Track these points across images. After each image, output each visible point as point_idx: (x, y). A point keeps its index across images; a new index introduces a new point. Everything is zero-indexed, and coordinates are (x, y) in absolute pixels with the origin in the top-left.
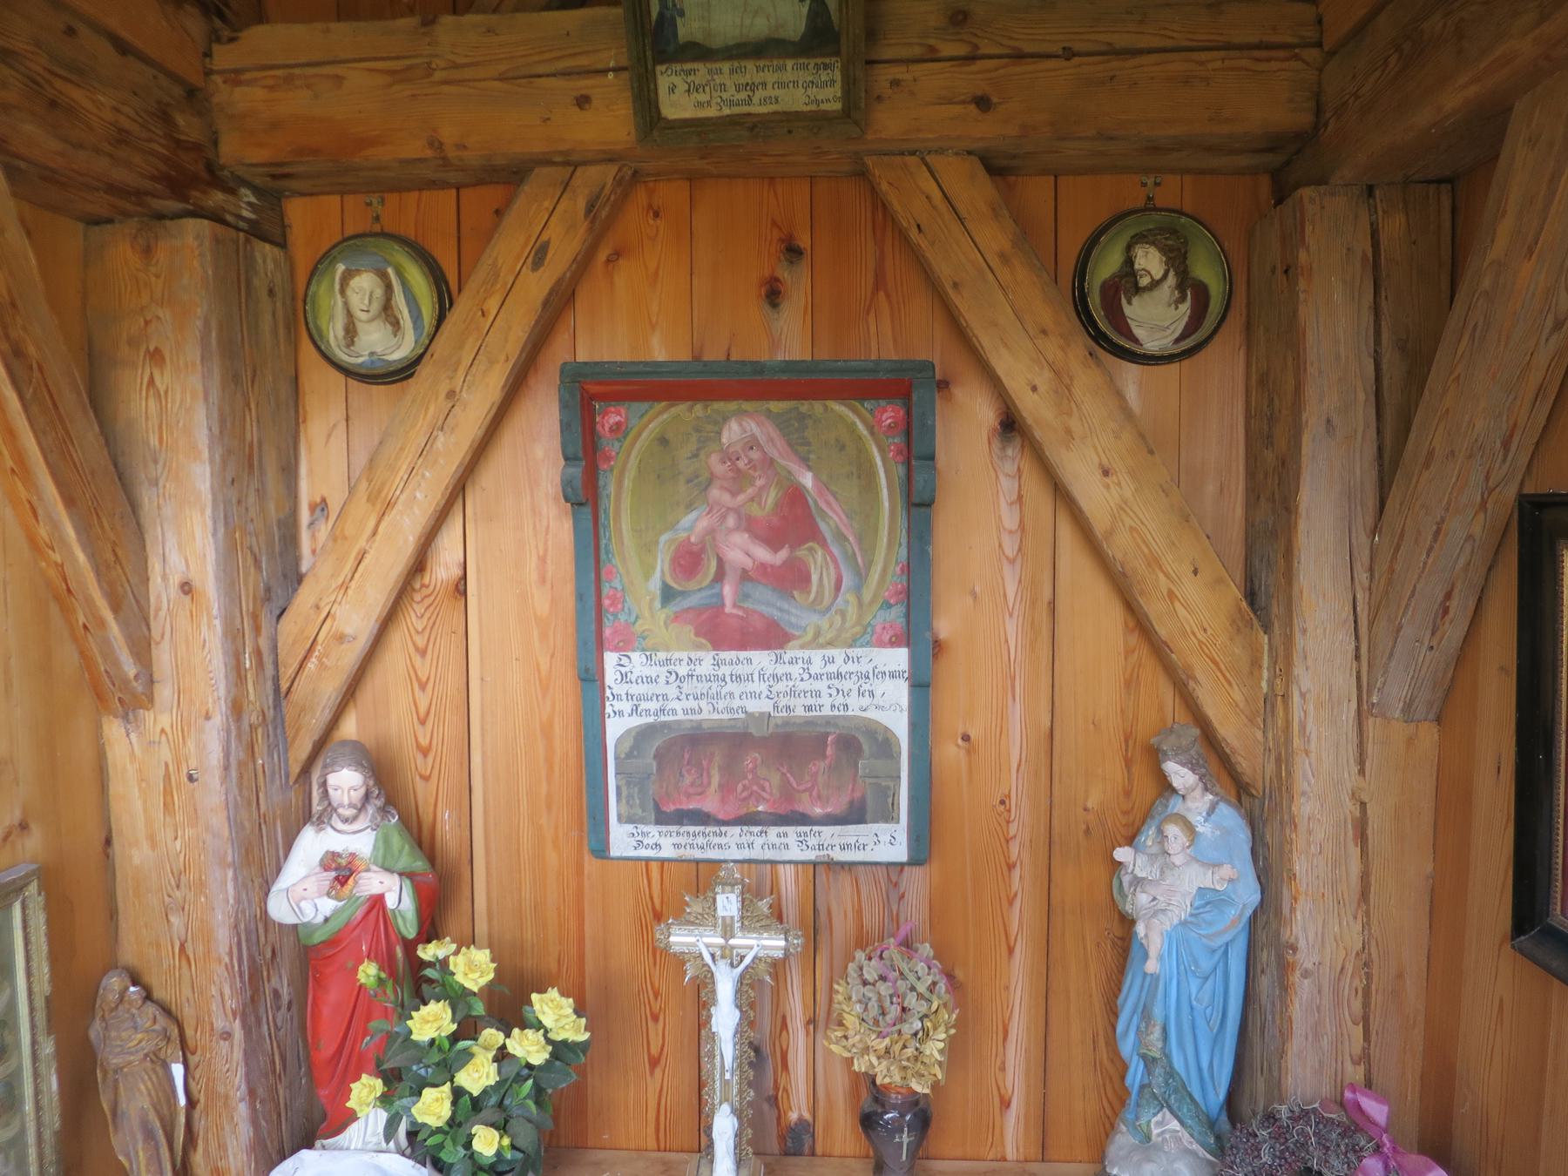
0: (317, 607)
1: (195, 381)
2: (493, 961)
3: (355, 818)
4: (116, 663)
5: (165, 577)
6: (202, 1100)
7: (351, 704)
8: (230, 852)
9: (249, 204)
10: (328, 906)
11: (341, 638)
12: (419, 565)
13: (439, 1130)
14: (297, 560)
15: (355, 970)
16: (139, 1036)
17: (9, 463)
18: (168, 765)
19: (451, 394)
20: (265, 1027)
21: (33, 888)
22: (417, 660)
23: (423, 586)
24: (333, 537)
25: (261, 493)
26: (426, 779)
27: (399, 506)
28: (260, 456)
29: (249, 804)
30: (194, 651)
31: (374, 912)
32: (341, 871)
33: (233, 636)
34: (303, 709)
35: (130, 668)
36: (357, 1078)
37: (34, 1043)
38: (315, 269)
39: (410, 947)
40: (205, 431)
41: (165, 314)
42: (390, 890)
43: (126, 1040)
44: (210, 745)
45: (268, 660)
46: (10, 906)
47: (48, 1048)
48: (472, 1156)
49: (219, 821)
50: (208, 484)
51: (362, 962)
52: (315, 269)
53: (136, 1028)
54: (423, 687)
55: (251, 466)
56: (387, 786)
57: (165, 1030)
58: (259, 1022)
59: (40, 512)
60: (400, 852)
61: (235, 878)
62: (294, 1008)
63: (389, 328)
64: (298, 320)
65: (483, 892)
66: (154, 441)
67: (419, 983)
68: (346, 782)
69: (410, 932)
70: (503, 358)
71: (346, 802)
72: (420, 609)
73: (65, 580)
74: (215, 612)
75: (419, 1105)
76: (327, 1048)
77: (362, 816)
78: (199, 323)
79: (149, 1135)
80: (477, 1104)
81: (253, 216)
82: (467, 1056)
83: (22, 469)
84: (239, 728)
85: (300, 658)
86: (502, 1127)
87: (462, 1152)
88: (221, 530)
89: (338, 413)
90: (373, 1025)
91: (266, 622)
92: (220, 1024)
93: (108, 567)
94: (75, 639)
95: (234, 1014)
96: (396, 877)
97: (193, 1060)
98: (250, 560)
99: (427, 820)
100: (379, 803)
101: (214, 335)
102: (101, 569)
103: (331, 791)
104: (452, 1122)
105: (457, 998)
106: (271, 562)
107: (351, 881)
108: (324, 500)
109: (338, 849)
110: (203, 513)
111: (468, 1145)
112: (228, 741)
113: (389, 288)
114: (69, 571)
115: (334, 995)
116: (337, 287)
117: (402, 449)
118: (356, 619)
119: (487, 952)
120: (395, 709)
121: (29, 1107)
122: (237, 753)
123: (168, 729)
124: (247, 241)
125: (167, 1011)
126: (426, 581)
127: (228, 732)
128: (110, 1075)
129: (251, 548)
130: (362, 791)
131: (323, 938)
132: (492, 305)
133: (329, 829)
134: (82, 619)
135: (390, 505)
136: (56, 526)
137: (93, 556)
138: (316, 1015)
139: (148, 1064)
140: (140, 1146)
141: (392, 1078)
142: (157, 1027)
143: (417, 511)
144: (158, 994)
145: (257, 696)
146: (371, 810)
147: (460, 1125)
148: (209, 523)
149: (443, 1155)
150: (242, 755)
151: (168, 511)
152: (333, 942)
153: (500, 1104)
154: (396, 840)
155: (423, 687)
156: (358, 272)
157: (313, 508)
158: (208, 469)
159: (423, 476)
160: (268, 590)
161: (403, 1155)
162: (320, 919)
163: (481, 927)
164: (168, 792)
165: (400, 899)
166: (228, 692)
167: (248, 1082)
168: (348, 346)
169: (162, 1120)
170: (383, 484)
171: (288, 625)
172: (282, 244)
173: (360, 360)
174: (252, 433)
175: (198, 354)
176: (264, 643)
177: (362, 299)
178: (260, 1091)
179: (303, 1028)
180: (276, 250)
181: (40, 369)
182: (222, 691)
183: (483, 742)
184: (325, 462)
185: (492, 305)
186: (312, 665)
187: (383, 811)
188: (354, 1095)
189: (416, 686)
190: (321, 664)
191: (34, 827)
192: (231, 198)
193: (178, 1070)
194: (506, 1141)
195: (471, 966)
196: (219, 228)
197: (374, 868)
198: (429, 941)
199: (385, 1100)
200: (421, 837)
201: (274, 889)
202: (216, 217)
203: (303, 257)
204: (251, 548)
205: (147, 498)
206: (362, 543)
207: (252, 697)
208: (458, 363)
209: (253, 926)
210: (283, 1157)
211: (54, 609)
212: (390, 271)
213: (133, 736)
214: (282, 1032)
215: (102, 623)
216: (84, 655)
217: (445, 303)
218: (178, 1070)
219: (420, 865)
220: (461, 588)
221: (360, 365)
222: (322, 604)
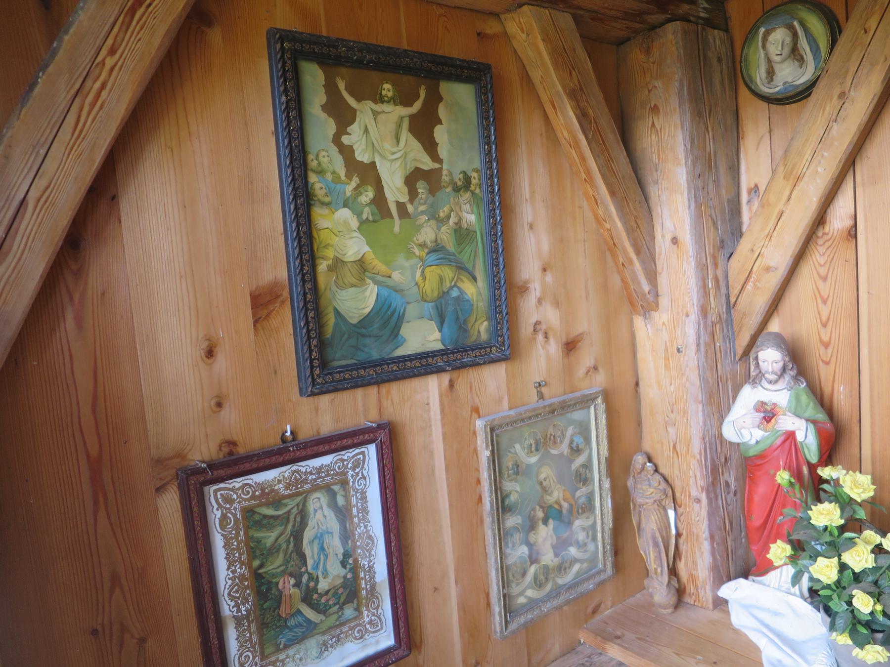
0: (752, 250)
1: (676, 119)
2: (873, 484)
3: (776, 382)
4: (639, 284)
5: (663, 236)
6: (684, 533)
7: (775, 313)
8: (700, 395)
9: (704, 8)
10: (759, 434)
11: (768, 269)
12: (820, 220)
13: (828, 587)
14: (740, 225)
15: (775, 475)
16: (652, 490)
17: (584, 176)
18: (667, 346)
19: (842, 95)
20: (720, 502)
21: (599, 400)
22: (821, 284)
23: (824, 234)
24: (762, 206)
25: (716, 182)
26: (827, 363)
27: (806, 179)
28: (717, 166)
29: (712, 369)
30: (679, 272)
31: (789, 440)
32: (768, 414)
33: (702, 267)
34: (744, 314)
35: (646, 287)
36: (775, 542)
37: (600, 480)
38: (747, 38)
39: (812, 468)
40: (682, 147)
41: (658, 84)
42: (799, 429)
43: (646, 492)
44: (689, 332)
45: (723, 283)
46: (589, 407)
47: (607, 484)
48: (852, 611)
49: (694, 377)
50: (685, 178)
51: (778, 470)
52: (747, 38)
53: (650, 485)
54: (825, 302)
55: (710, 166)
56: (797, 361)
57: (665, 490)
58: (717, 498)
59: (599, 201)
60: (807, 406)
61: (703, 411)
62: (738, 495)
63: (796, 63)
64: (737, 74)
65: (868, 439)
66: (655, 158)
67: (818, 489)
68: (770, 357)
69: (814, 459)
70: (882, 59)
71: (770, 370)
72: (822, 250)
73: (612, 238)
74: (691, 253)
75: (815, 566)
76: (757, 520)
77: (781, 381)
78: (677, 84)
79: (656, 544)
80: (857, 578)
81: (707, 16)
82: (851, 543)
83: (590, 179)
84: (705, 323)
85: (742, 282)
86: (878, 596)
87: (845, 607)
88: (693, 205)
89: (764, 128)
90: (785, 511)
91: (721, 261)
92: (694, 493)
93: (633, 230)
94: (619, 272)
95: (702, 489)
96: (804, 422)
97: (680, 510)
98: (710, 223)
99: (827, 390)
100: (793, 373)
101: (685, 88)
102: (630, 231)
103: (760, 363)
104: (838, 583)
105: (846, 504)
106: (724, 225)
107: (773, 421)
108: (756, 186)
109: (766, 400)
110: (682, 195)
111: (849, 603)
112: (699, 330)
113: (795, 35)
114: (614, 234)
115: (762, 490)
116: (760, 44)
117: (807, 140)
118: (779, 257)
119: (869, 477)
120: (802, 316)
121: (598, 512)
122: (705, 338)
123: (666, 322)
124: (703, 29)
125: (666, 480)
126: (827, 230)
127: (699, 324)
128: (637, 507)
129: (711, 216)
130: (781, 364)
131: (755, 453)
132: (873, 24)
133: (760, 387)
134: (621, 260)
135: (799, 179)
136: (606, 208)
137: (625, 223)
138: (750, 500)
139: (656, 506)
140: (651, 548)
141: (798, 547)
142: (660, 487)
143: (818, 180)
144: (662, 470)
145: (716, 305)
146: (787, 378)
147: (844, 588)
148: (686, 201)
149: (831, 604)
150: (707, 339)
151: (664, 197)
152: (762, 456)
153: (876, 583)
154: (804, 398)
155: (825, 302)
156: (773, 29)
157: (750, 191)
158: (685, 169)
159: (823, 156)
160: (722, 241)
161: (805, 600)
162: (753, 442)
163: (867, 464)
164: (667, 359)
165: (808, 439)
166: (699, 301)
167: (710, 530)
168: (769, 83)
169: (663, 542)
170: (794, 165)
171: (734, 263)
172: (726, 30)
173: (777, 89)
174: (711, 146)
175: (677, 102)
176: (719, 273)
177: (777, 47)
178: (717, 537)
179: (743, 508)
180: (721, 33)
181: (596, 123)
182: (695, 301)
183: (870, 339)
184: (756, 165)
185: (873, 24)
186: (749, 287)
187: (795, 378)
188: (771, 551)
189: (820, 301)
190: (756, 287)
191: (600, 369)
192: (693, 7)
193: (671, 514)
194: (879, 608)
195: (856, 484)
196: (685, 24)
197: (789, 414)
198: (826, 466)
199: (793, 559)
200: (823, 401)
201: (726, 420)
202: (685, 19)
203: (738, 33)
204: (711, 216)
205: (652, 191)
206: (780, 207)
207: (713, 306)
208: (847, 72)
209: (713, 441)
210: (730, 579)
211: (608, 256)
212: (796, 23)
213: (648, 326)
214: (730, 507)
215: (631, 262)
216: (624, 281)
217: (835, 31)
218: (671, 514)
219: (821, 416)
220: (853, 233)
221: (777, 93)
222: (755, 248)
